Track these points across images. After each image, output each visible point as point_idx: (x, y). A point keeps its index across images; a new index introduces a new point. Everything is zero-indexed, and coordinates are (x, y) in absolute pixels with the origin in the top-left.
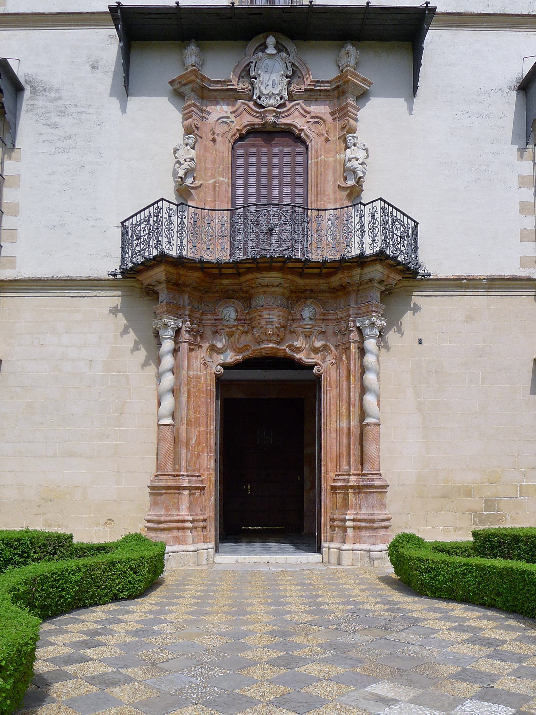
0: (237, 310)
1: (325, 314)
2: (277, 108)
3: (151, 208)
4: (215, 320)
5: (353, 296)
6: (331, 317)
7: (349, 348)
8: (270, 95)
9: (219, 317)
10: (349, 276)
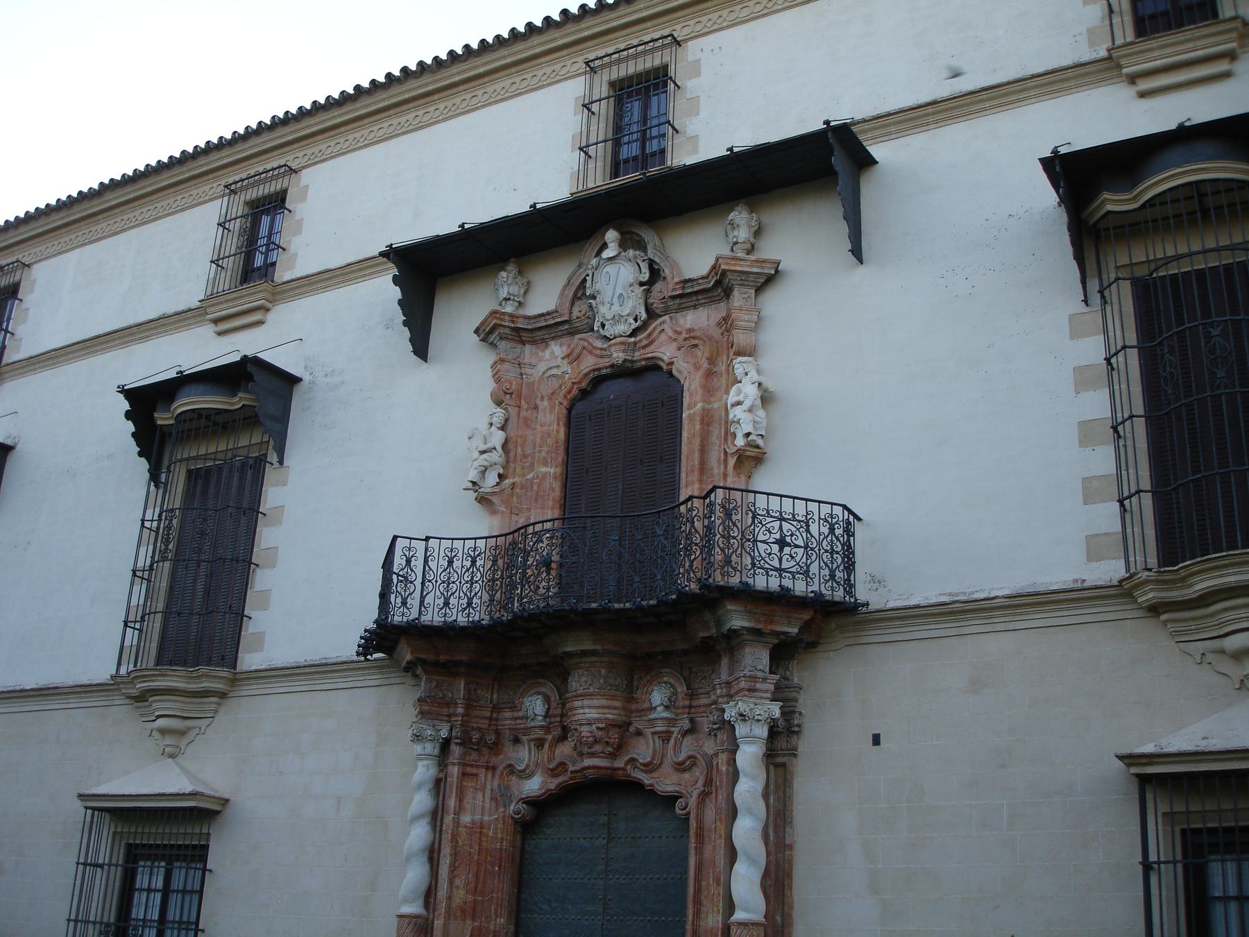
2: (630, 336)
4: (516, 719)
8: (617, 319)
9: (521, 714)
10: (436, 664)
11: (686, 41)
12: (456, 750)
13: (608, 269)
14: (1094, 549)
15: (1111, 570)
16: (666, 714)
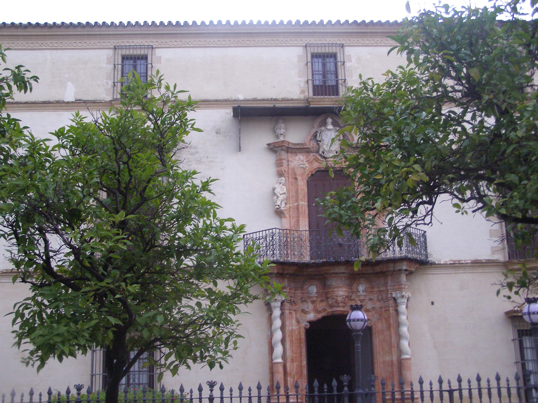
0: (317, 287)
1: (373, 288)
3: (267, 232)
5: (389, 278)
6: (376, 289)
7: (389, 310)
9: (306, 292)
11: (156, 48)
12: (287, 305)
13: (327, 132)
14: (494, 251)
16: (364, 294)
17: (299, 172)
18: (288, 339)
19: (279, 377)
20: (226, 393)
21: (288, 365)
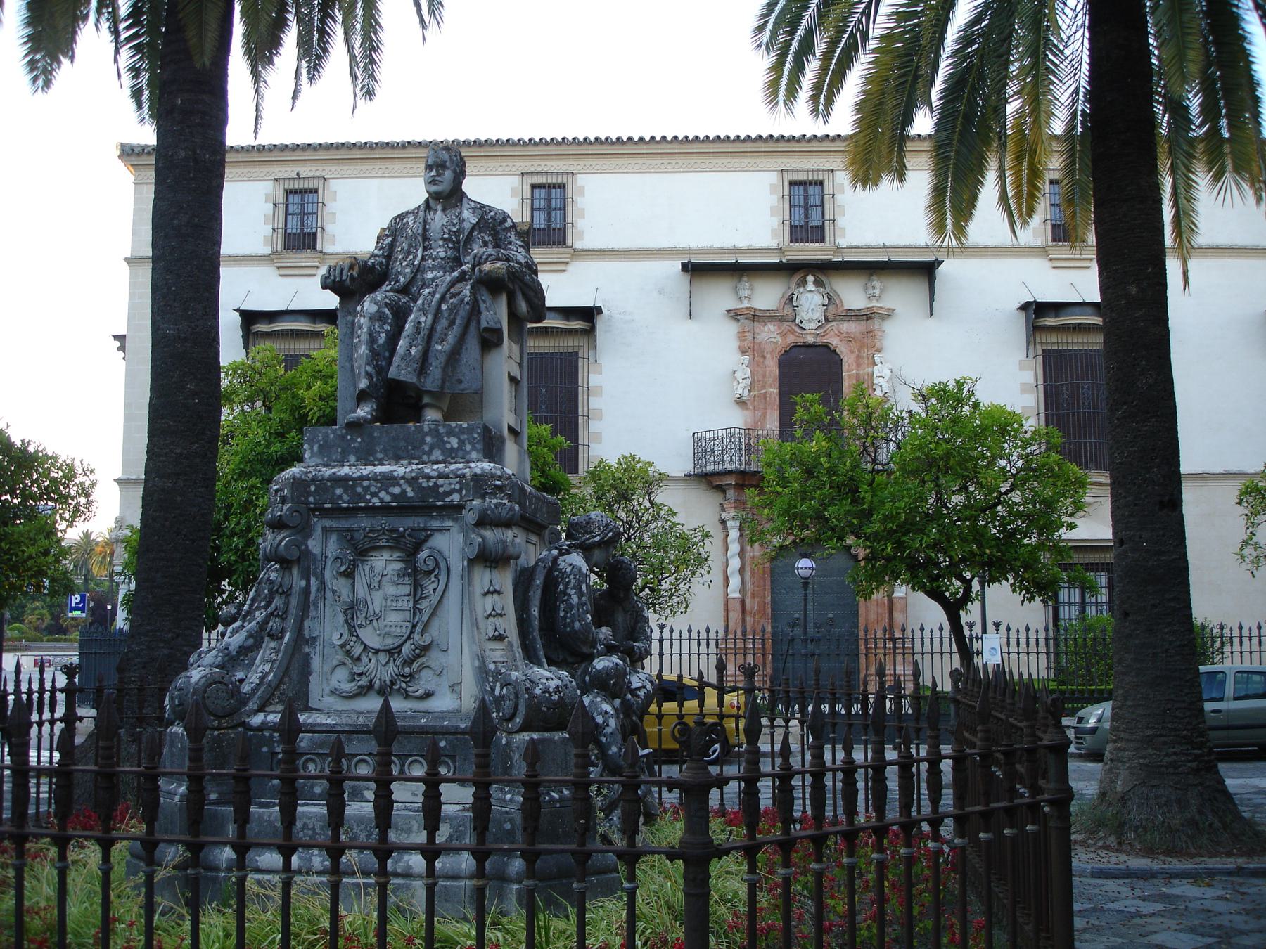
8: (810, 320)
15: (268, 250)
17: (768, 348)
18: (748, 568)
19: (735, 616)
20: (676, 635)
21: (748, 601)
